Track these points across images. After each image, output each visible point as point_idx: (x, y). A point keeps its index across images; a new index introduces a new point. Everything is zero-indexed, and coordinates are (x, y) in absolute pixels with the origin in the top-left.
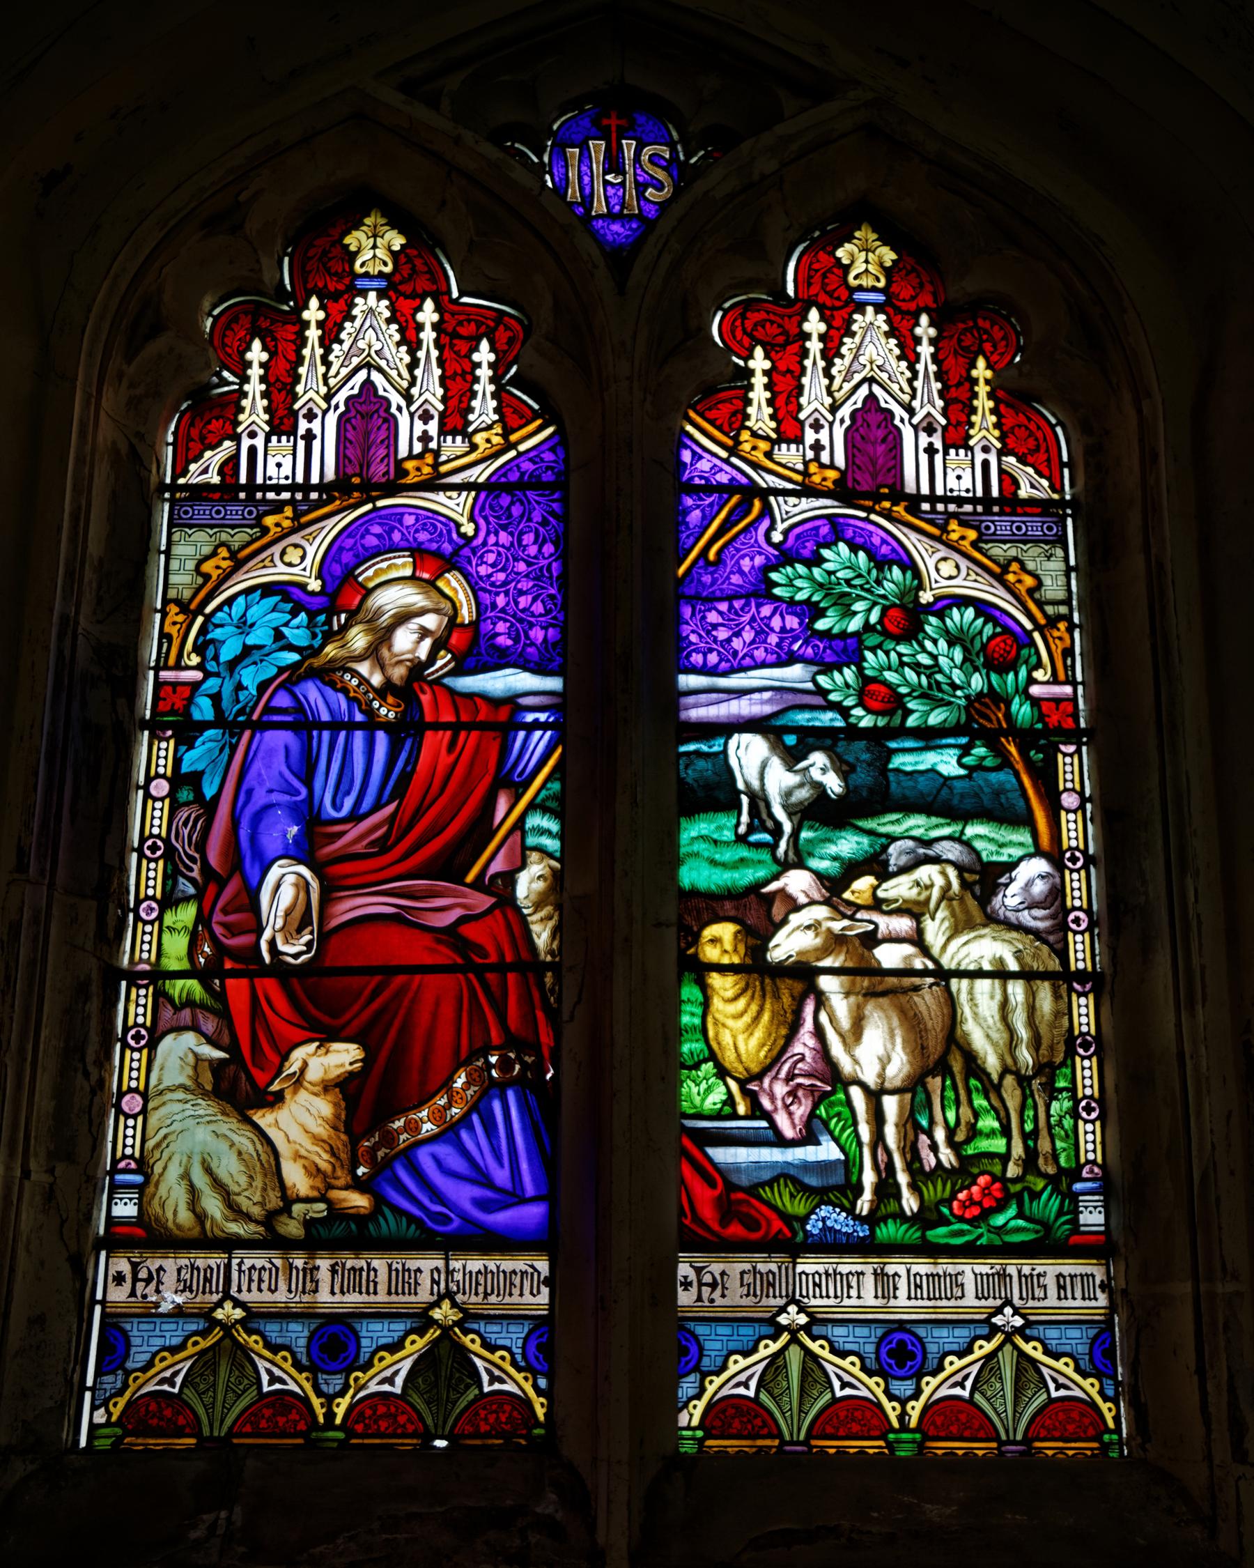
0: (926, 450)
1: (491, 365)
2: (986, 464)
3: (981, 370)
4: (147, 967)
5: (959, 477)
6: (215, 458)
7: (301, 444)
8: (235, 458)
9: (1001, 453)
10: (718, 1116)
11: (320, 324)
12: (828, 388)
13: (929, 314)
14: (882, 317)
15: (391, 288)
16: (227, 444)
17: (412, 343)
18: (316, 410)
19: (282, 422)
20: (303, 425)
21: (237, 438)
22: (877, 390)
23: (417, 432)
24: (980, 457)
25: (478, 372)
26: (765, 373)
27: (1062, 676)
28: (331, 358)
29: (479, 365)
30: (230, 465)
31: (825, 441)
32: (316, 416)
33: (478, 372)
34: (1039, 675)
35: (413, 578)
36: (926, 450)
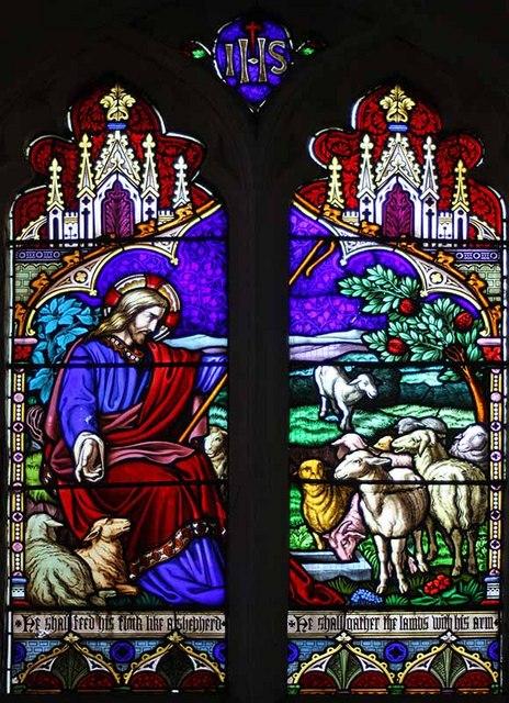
0: (147, 213)
2: (460, 221)
3: (460, 168)
6: (35, 225)
7: (82, 217)
8: (46, 225)
9: (469, 215)
10: (308, 550)
11: (89, 150)
12: (93, 179)
16: (42, 217)
19: (71, 204)
21: (47, 214)
24: (457, 216)
25: (178, 175)
26: (338, 172)
28: (96, 169)
29: (178, 171)
33: (178, 175)
34: (483, 333)
36: (147, 213)
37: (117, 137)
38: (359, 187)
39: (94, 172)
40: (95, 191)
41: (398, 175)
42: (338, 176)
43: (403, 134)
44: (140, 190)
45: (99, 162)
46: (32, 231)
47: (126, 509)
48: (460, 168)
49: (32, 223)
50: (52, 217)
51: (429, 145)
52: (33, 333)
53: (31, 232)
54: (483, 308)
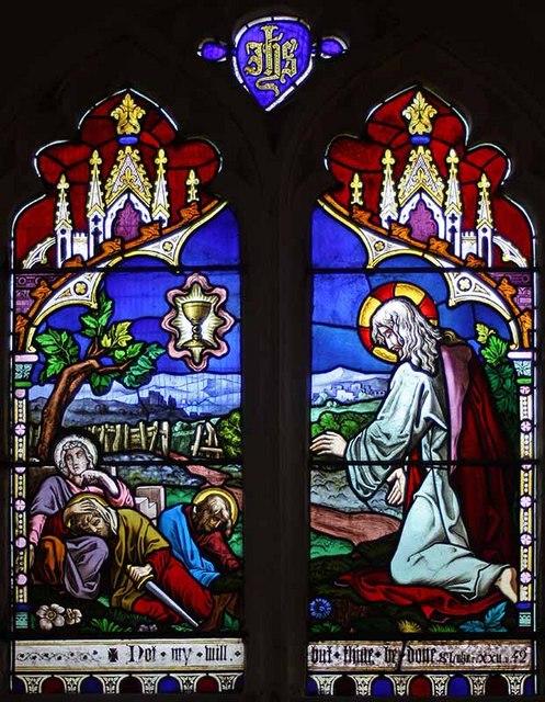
1: (488, 189)
2: (485, 239)
3: (484, 183)
4: (524, 466)
5: (467, 246)
6: (42, 248)
7: (92, 237)
9: (494, 233)
10: (14, 523)
12: (103, 197)
13: (455, 149)
14: (428, 152)
15: (430, 141)
16: (49, 239)
17: (152, 177)
18: (99, 216)
19: (80, 225)
20: (92, 226)
21: (54, 235)
22: (424, 197)
23: (449, 227)
24: (481, 235)
25: (481, 194)
27: (526, 345)
28: (399, 187)
29: (481, 189)
30: (51, 252)
31: (101, 229)
32: (100, 220)
33: (481, 194)
34: (512, 347)
35: (417, 307)
37: (421, 155)
38: (89, 206)
39: (397, 191)
40: (106, 210)
41: (129, 191)
42: (360, 194)
43: (426, 147)
44: (443, 208)
45: (402, 179)
46: (37, 255)
47: (417, 477)
48: (484, 183)
49: (39, 246)
50: (60, 236)
51: (161, 159)
52: (34, 350)
53: (38, 255)
54: (30, 324)
